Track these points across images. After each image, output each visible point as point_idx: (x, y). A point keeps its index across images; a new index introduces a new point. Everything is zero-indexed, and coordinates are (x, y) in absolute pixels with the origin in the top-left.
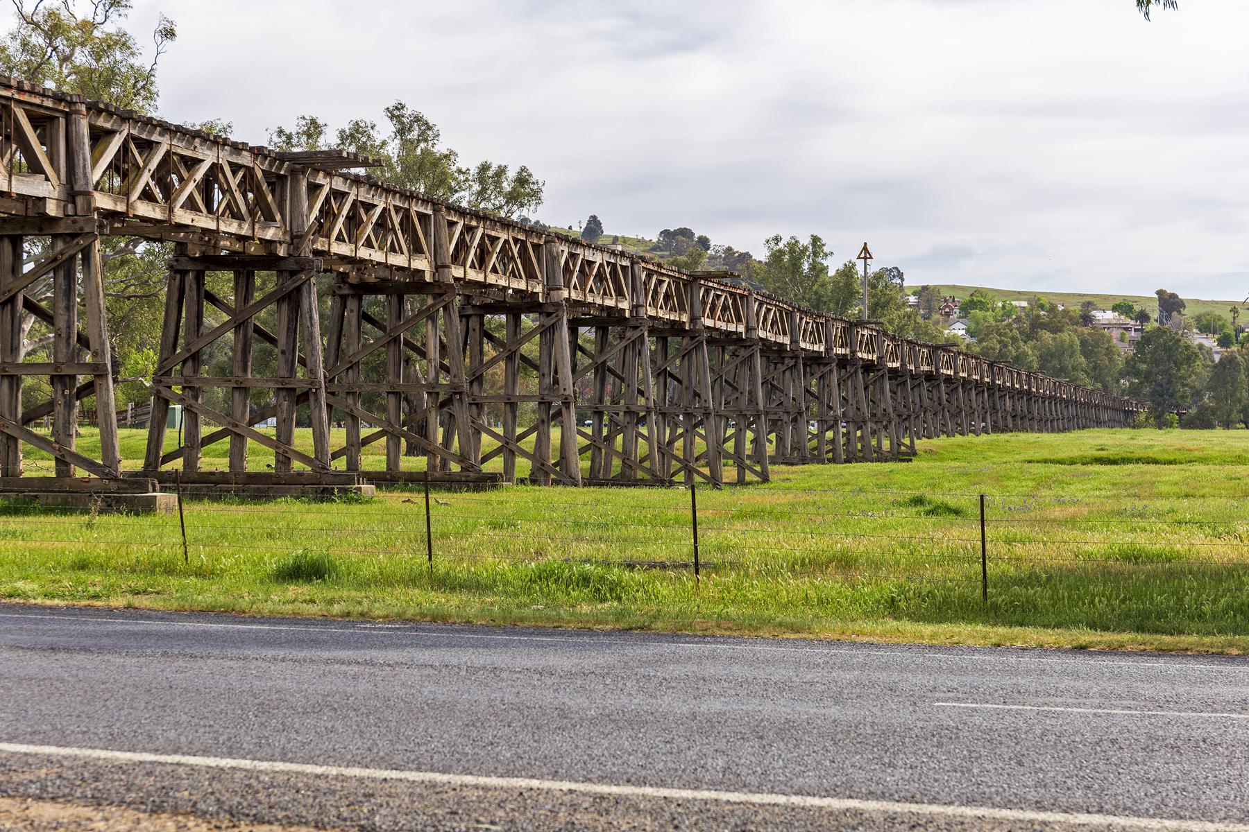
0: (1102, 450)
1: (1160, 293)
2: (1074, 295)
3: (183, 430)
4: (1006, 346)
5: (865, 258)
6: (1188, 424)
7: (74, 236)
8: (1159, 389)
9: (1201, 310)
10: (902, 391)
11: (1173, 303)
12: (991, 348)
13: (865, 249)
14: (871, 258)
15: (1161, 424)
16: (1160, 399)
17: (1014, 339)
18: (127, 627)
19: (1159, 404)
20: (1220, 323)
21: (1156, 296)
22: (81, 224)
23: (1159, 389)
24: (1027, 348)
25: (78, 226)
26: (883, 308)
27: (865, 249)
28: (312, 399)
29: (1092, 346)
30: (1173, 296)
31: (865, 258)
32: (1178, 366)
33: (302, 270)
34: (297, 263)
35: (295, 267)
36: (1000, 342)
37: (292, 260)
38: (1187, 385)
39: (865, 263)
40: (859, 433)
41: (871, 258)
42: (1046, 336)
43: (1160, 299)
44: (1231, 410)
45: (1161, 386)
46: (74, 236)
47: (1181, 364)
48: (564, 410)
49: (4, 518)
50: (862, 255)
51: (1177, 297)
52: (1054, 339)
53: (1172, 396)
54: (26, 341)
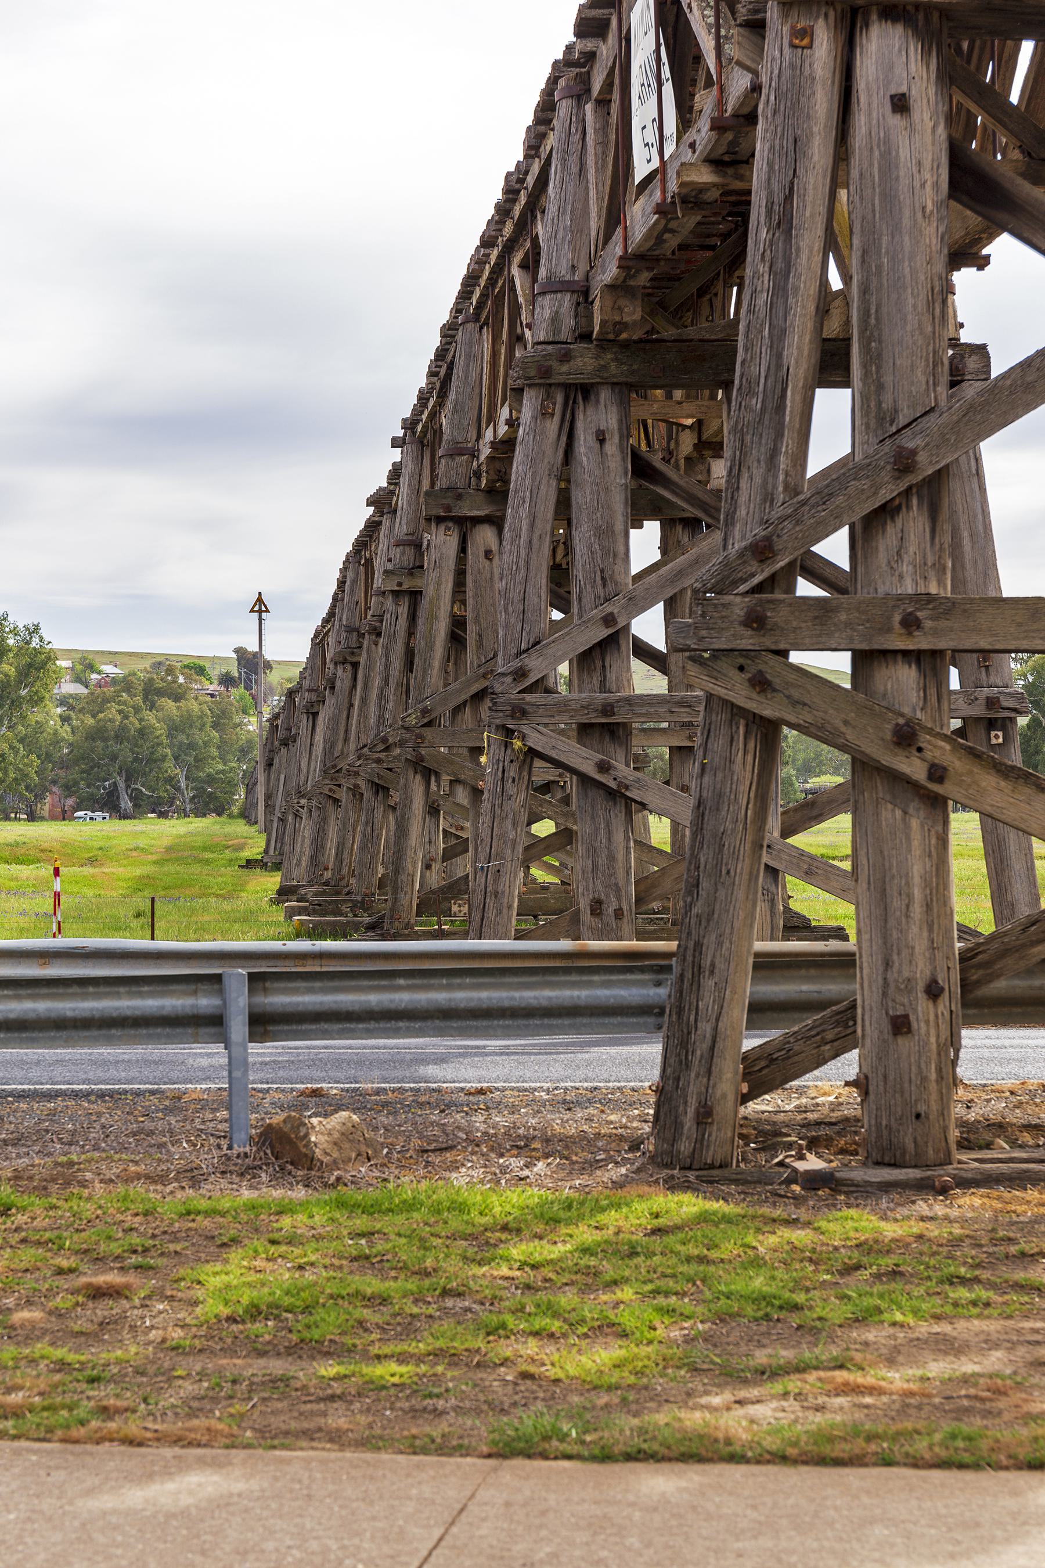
2: (103, 652)
3: (754, 788)
4: (126, 717)
5: (260, 611)
10: (343, 755)
12: (110, 720)
13: (260, 600)
14: (267, 611)
17: (137, 710)
18: (865, 965)
21: (235, 656)
24: (150, 717)
26: (38, 669)
27: (260, 600)
31: (260, 611)
36: (120, 712)
39: (260, 619)
41: (267, 611)
42: (168, 704)
50: (257, 608)
52: (178, 708)
54: (380, 867)
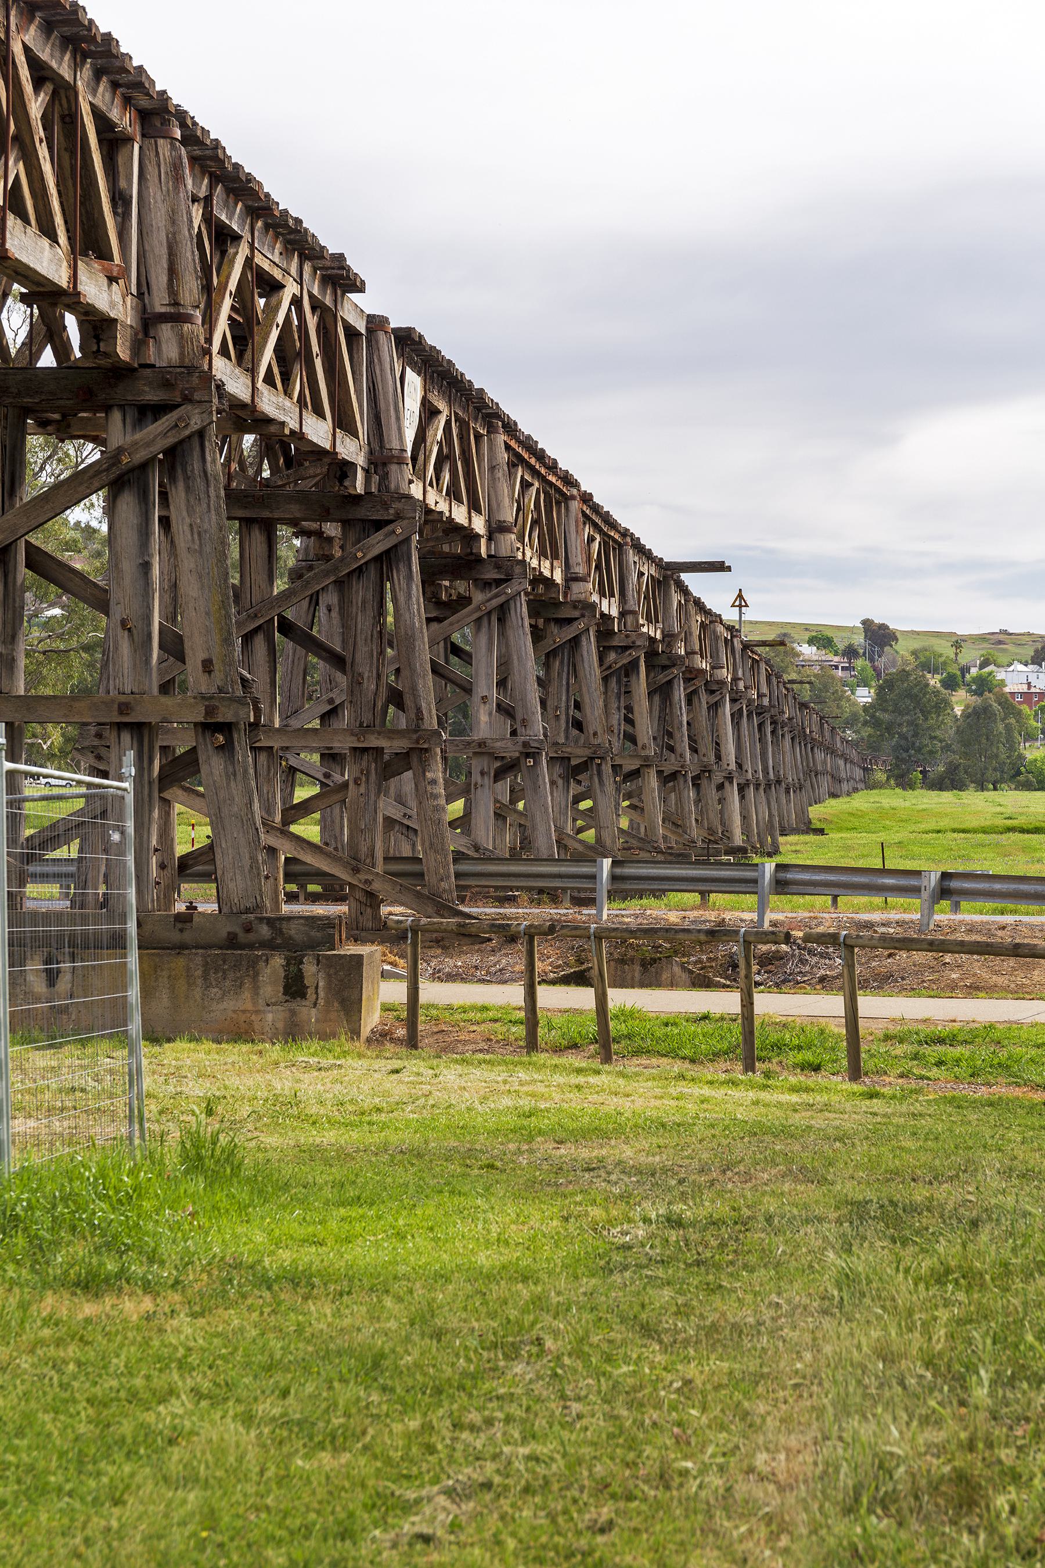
0: (1010, 818)
1: (867, 623)
5: (740, 606)
6: (939, 785)
7: (626, 648)
8: (903, 742)
9: (916, 645)
11: (884, 636)
13: (740, 596)
15: (904, 782)
16: (904, 755)
19: (903, 761)
20: (941, 660)
22: (634, 638)
23: (903, 742)
25: (630, 640)
27: (740, 596)
28: (681, 780)
29: (820, 690)
30: (883, 627)
31: (740, 606)
32: (926, 714)
33: (674, 665)
34: (669, 658)
35: (667, 663)
37: (665, 656)
38: (935, 738)
40: (457, 807)
43: (866, 631)
44: (986, 768)
45: (906, 739)
46: (626, 648)
47: (929, 712)
48: (727, 784)
49: (1044, 875)
51: (887, 627)
53: (919, 750)
